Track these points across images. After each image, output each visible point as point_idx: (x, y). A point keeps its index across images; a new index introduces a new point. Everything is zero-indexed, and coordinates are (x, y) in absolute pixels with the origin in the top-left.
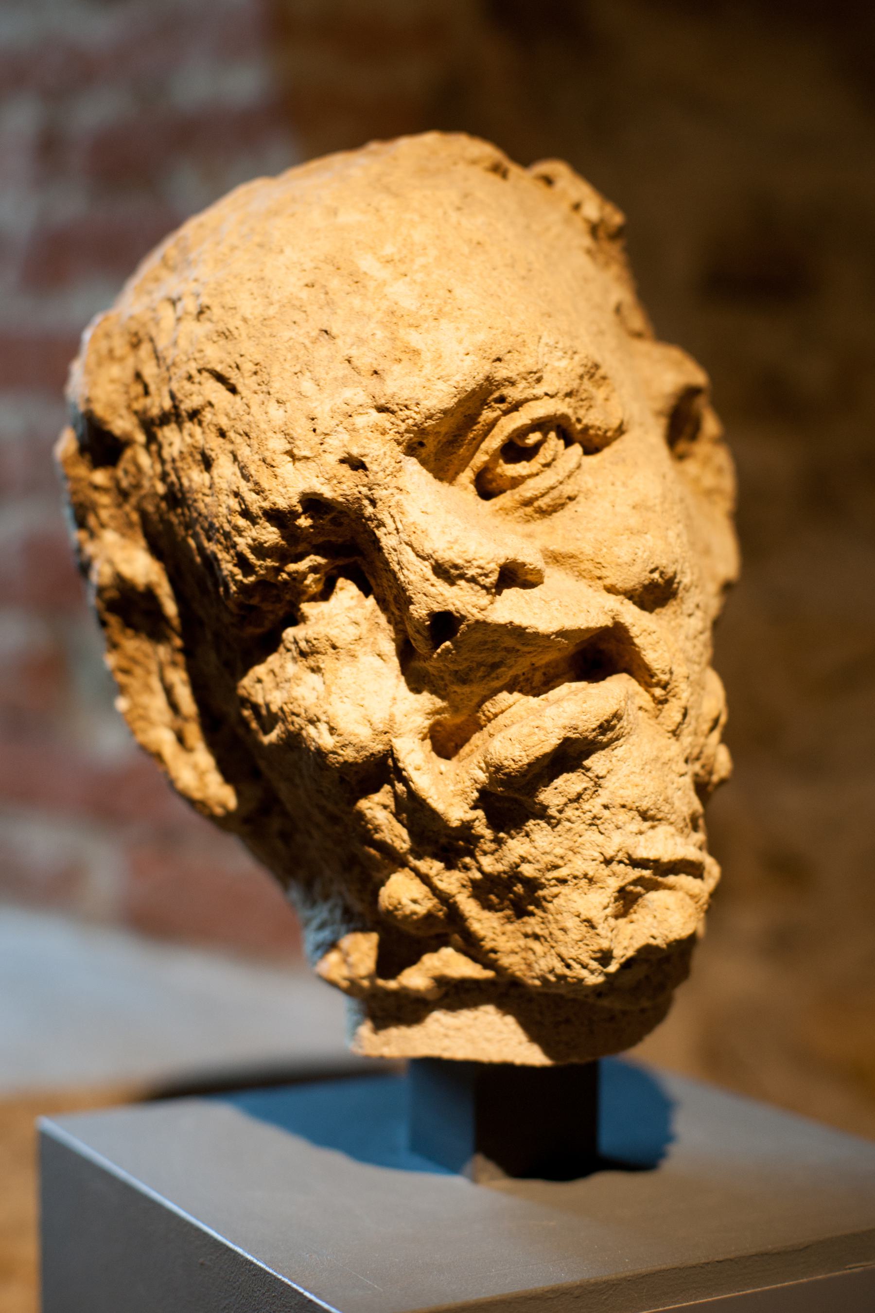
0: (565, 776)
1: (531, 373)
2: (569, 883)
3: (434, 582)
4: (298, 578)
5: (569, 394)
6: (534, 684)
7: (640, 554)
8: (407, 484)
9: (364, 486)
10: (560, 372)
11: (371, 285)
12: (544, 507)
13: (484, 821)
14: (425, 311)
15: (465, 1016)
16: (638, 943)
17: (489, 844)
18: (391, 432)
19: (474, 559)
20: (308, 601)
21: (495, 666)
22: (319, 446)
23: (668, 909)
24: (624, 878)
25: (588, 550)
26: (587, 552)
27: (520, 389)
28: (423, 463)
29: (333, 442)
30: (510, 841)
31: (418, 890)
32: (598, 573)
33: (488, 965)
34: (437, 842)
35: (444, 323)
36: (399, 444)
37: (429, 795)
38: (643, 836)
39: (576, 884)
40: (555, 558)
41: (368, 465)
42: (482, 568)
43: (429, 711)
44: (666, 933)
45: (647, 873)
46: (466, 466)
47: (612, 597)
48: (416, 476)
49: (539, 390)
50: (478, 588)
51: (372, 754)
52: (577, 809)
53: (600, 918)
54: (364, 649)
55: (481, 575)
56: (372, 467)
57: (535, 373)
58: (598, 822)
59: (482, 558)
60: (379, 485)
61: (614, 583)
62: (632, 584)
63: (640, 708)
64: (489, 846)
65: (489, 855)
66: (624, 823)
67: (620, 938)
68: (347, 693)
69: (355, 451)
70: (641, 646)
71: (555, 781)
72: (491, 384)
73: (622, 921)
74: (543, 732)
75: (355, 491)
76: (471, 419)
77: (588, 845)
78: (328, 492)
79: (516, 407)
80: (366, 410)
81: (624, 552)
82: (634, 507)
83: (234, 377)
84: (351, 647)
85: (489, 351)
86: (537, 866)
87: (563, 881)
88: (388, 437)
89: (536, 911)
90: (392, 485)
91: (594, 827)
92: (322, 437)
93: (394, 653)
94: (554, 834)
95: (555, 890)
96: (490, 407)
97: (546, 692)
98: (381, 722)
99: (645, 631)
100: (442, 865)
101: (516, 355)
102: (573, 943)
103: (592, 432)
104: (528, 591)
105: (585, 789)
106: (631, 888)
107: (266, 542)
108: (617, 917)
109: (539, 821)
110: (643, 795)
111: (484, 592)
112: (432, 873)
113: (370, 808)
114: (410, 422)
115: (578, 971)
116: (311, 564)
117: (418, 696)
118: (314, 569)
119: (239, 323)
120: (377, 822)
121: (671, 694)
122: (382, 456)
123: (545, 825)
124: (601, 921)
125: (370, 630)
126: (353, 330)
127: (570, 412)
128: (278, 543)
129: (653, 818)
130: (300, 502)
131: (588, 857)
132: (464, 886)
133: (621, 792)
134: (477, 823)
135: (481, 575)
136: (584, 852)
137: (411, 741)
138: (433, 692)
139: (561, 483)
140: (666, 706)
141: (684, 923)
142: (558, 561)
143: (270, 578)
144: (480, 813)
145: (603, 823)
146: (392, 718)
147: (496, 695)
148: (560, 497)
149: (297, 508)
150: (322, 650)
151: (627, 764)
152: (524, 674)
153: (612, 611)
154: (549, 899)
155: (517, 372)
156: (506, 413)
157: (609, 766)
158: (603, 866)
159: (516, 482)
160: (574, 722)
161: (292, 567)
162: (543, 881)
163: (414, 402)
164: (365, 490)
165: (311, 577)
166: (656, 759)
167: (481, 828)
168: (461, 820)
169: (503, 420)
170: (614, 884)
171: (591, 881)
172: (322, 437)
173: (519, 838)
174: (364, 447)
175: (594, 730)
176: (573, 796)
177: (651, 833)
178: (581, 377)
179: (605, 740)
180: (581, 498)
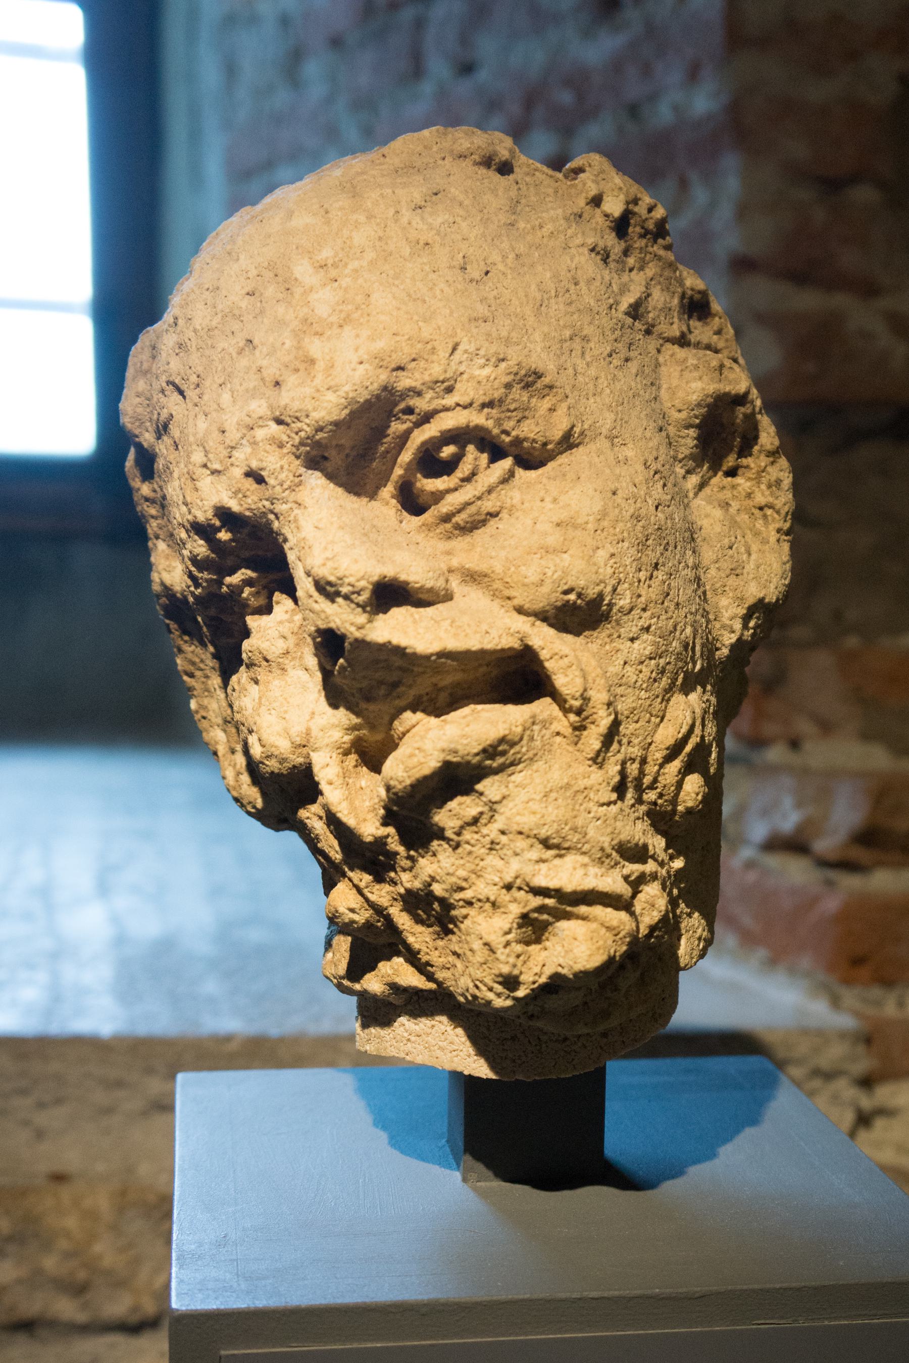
0: (459, 799)
1: (437, 382)
2: (475, 905)
3: (317, 599)
4: (236, 591)
5: (490, 404)
6: (438, 705)
7: (550, 573)
8: (306, 499)
9: (267, 500)
10: (479, 378)
11: (298, 291)
12: (462, 523)
13: (397, 837)
14: (334, 319)
15: (423, 1024)
16: (548, 971)
17: (405, 861)
18: (289, 445)
19: (345, 576)
20: (253, 614)
21: (395, 685)
22: (228, 459)
23: (575, 939)
24: (524, 907)
25: (499, 568)
26: (497, 571)
27: (427, 400)
28: (330, 477)
29: (238, 455)
30: (420, 859)
31: (354, 900)
32: (507, 593)
33: (430, 977)
34: (363, 855)
35: (347, 328)
36: (297, 457)
37: (339, 809)
38: (546, 864)
39: (481, 907)
40: (473, 577)
41: (267, 479)
42: (353, 586)
43: (346, 726)
44: (571, 963)
45: (550, 902)
46: (388, 480)
47: (523, 618)
48: (318, 491)
49: (449, 401)
50: (353, 606)
51: (294, 767)
52: (476, 833)
53: (499, 944)
54: (292, 663)
55: (353, 593)
56: (271, 481)
57: (443, 382)
58: (498, 847)
59: (351, 575)
60: (278, 500)
61: (522, 603)
62: (541, 605)
63: (558, 734)
64: (407, 863)
65: (408, 872)
66: (523, 850)
67: (530, 964)
68: (275, 705)
69: (254, 465)
70: (551, 670)
71: (449, 803)
72: (393, 395)
73: (534, 948)
74: (422, 754)
75: (260, 505)
76: (380, 432)
77: (489, 869)
78: (234, 506)
79: (427, 418)
80: (266, 423)
81: (531, 573)
82: (558, 525)
83: (184, 387)
84: (281, 660)
85: (388, 359)
86: (444, 886)
87: (470, 903)
88: (285, 450)
89: (455, 930)
90: (291, 499)
91: (494, 852)
92: (229, 450)
93: (317, 668)
94: (456, 856)
95: (464, 911)
96: (399, 419)
97: (448, 713)
98: (298, 736)
99: (556, 654)
100: (371, 878)
101: (422, 364)
102: (478, 965)
103: (526, 444)
104: (421, 610)
105: (481, 813)
106: (536, 915)
107: (198, 555)
108: (528, 943)
109: (442, 843)
110: (542, 822)
111: (360, 610)
112: (362, 885)
113: (308, 818)
114: (302, 434)
115: (484, 993)
116: (243, 577)
117: (335, 712)
118: (248, 582)
119: (191, 334)
120: (317, 832)
121: (588, 721)
122: (278, 469)
123: (446, 846)
124: (501, 946)
125: (297, 645)
126: (271, 339)
127: (490, 424)
128: (208, 556)
129: (557, 847)
130: (215, 515)
131: (490, 882)
132: (396, 900)
133: (518, 818)
134: (389, 840)
135: (353, 593)
136: (487, 876)
137: (328, 755)
138: (349, 708)
139: (479, 498)
140: (585, 733)
141: (590, 956)
142: (475, 580)
143: (214, 589)
144: (391, 830)
145: (501, 849)
146: (308, 733)
147: (401, 714)
148: (478, 513)
149: (213, 522)
150: (257, 662)
151: (526, 790)
152: (427, 694)
153: (518, 632)
154: (461, 919)
155: (421, 381)
156: (418, 424)
157: (504, 791)
158: (504, 891)
159: (438, 497)
160: (452, 746)
161: (228, 580)
162: (452, 901)
163: (304, 414)
164: (267, 504)
165: (247, 592)
166: (568, 786)
167: (395, 845)
168: (373, 836)
169: (416, 432)
170: (516, 910)
171: (494, 904)
172: (229, 450)
173: (428, 856)
174: (262, 461)
175: (477, 754)
176: (468, 819)
177: (557, 861)
178: (508, 386)
179: (495, 765)
180: (504, 515)
